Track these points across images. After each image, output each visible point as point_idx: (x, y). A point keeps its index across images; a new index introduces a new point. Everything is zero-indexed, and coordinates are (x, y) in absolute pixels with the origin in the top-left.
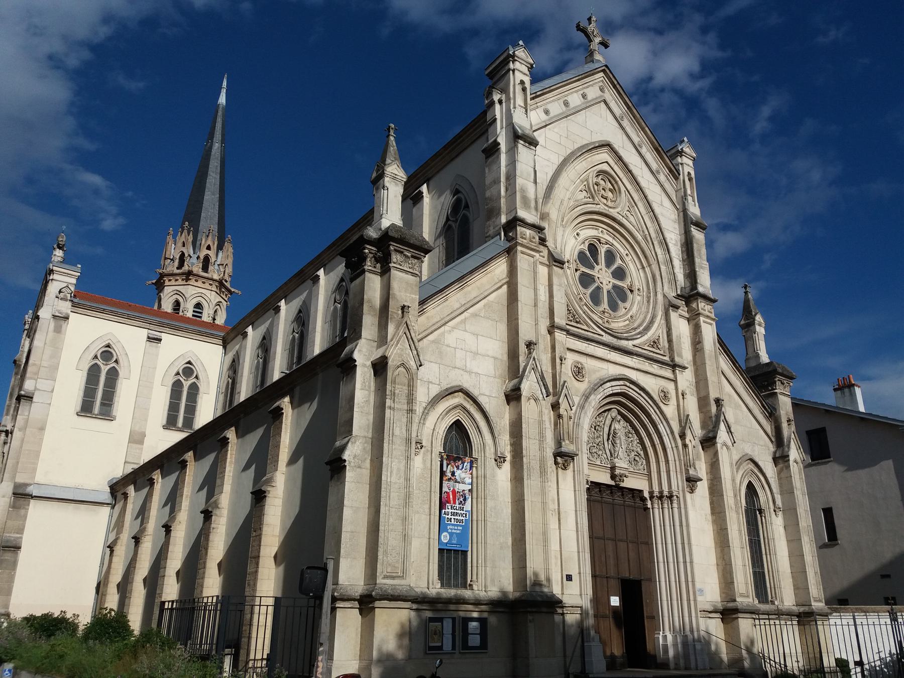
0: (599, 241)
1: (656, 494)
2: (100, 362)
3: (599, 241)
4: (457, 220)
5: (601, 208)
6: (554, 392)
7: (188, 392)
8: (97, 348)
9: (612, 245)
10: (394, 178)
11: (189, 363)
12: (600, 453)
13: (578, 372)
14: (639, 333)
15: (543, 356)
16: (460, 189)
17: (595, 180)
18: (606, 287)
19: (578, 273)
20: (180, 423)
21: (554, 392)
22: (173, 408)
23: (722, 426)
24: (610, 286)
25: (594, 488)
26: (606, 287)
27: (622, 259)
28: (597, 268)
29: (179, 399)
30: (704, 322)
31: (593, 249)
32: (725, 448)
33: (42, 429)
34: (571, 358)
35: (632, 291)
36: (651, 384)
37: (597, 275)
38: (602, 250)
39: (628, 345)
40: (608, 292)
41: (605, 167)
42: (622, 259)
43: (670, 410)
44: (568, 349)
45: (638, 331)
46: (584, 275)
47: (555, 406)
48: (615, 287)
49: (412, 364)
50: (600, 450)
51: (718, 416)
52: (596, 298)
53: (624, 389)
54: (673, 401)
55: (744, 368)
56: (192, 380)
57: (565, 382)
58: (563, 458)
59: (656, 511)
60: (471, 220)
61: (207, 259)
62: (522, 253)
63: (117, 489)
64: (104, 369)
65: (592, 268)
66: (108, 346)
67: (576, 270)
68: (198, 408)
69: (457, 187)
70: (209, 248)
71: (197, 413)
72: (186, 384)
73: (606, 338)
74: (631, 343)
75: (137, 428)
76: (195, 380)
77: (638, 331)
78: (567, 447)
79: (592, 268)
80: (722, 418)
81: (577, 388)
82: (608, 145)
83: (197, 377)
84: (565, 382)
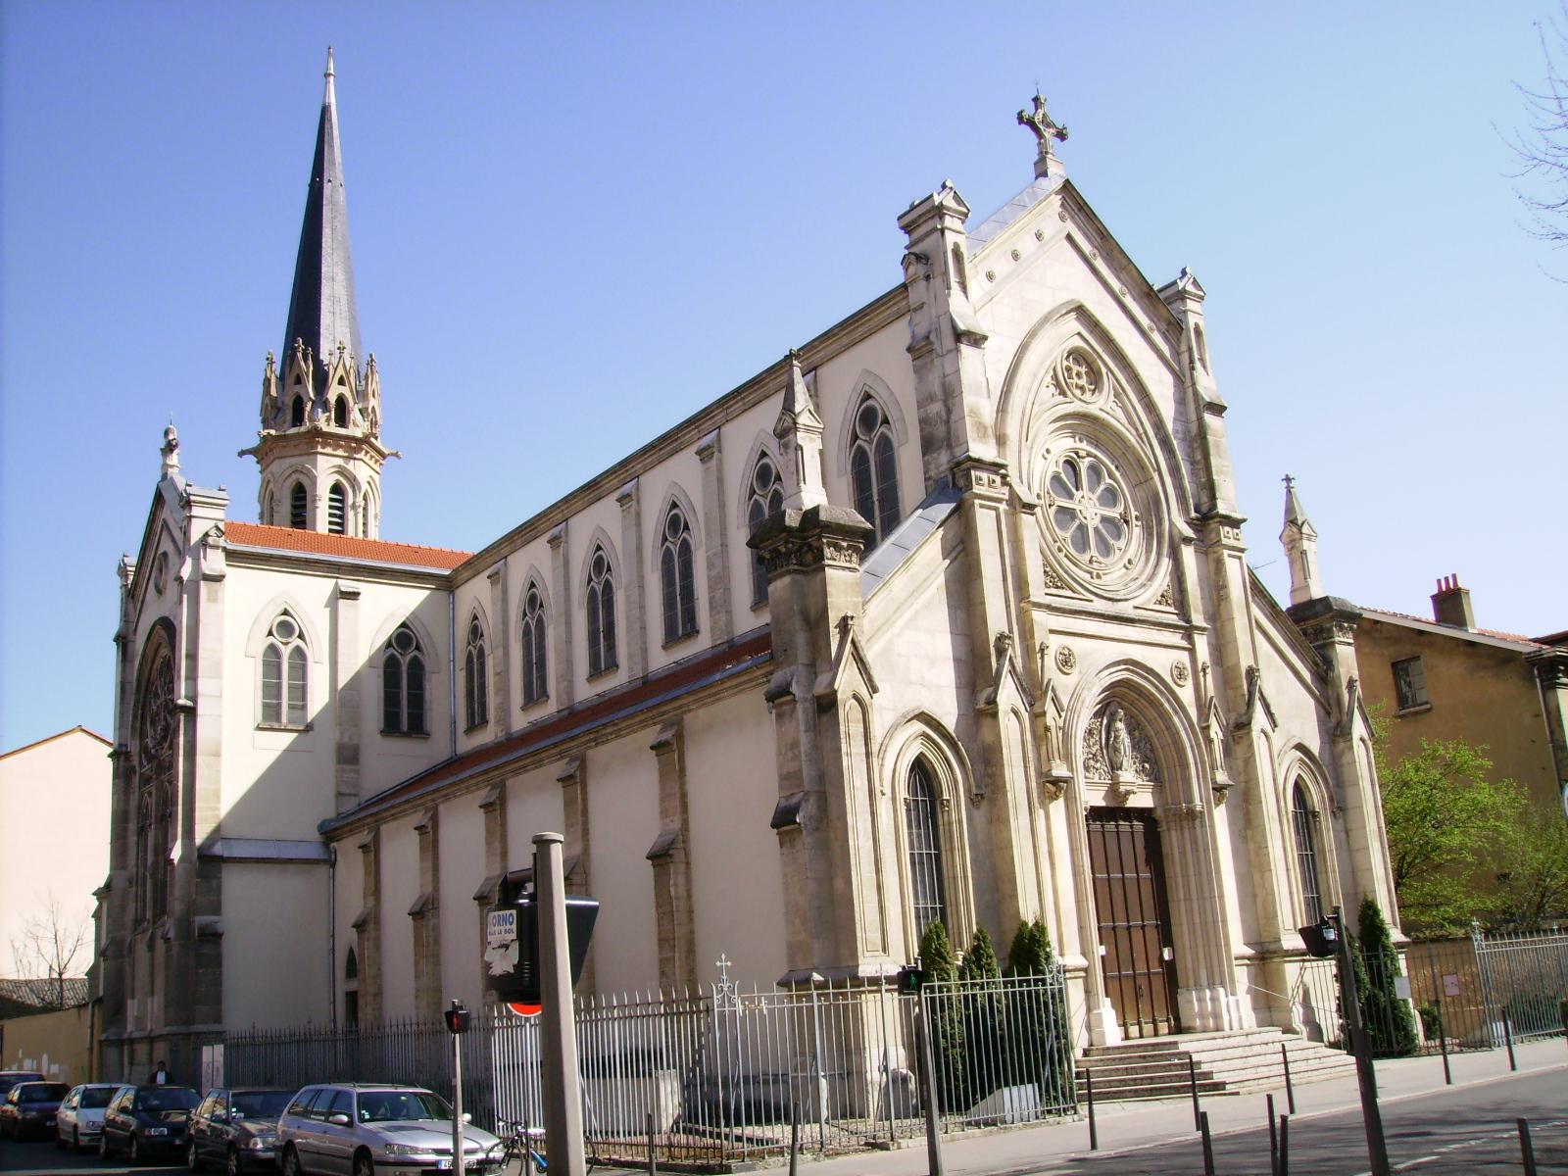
0: (1077, 453)
1: (1266, 956)
2: (277, 640)
3: (1077, 453)
4: (872, 440)
5: (1077, 407)
6: (1034, 690)
7: (408, 673)
8: (272, 618)
9: (1095, 457)
10: (808, 429)
11: (286, 613)
12: (1098, 765)
13: (1066, 661)
14: (1143, 585)
15: (1015, 651)
16: (872, 393)
17: (1065, 363)
18: (1093, 523)
19: (1054, 508)
20: (405, 726)
21: (1034, 690)
22: (271, 690)
23: (1258, 707)
24: (1098, 517)
25: (1095, 814)
26: (1093, 523)
27: (1111, 476)
28: (1078, 495)
29: (398, 685)
30: (1230, 556)
31: (1070, 464)
32: (1263, 735)
33: (217, 754)
34: (1055, 643)
35: (1126, 522)
36: (1161, 661)
37: (1077, 507)
38: (1083, 465)
39: (1125, 609)
40: (1096, 530)
41: (1080, 343)
42: (1111, 476)
43: (1186, 694)
44: (1052, 632)
45: (1139, 582)
46: (1062, 510)
47: (1037, 716)
48: (1105, 520)
49: (864, 692)
50: (1097, 761)
51: (1251, 694)
52: (1081, 543)
53: (1126, 675)
54: (1189, 683)
55: (1285, 603)
56: (412, 653)
57: (1049, 680)
58: (1053, 787)
59: (1173, 833)
60: (895, 444)
61: (341, 402)
62: (982, 506)
63: (330, 834)
64: (286, 652)
65: (1071, 496)
66: (286, 613)
67: (1050, 506)
68: (427, 697)
69: (867, 388)
70: (341, 382)
71: (427, 706)
72: (405, 662)
73: (1099, 605)
74: (1131, 603)
75: (346, 740)
76: (416, 653)
77: (1139, 582)
78: (1059, 770)
79: (1071, 496)
80: (1257, 695)
81: (1063, 684)
82: (1081, 311)
83: (418, 648)
84: (1049, 680)
